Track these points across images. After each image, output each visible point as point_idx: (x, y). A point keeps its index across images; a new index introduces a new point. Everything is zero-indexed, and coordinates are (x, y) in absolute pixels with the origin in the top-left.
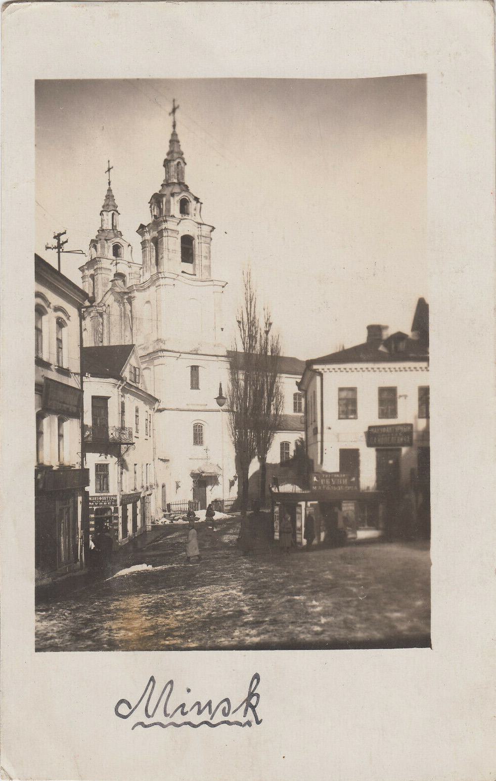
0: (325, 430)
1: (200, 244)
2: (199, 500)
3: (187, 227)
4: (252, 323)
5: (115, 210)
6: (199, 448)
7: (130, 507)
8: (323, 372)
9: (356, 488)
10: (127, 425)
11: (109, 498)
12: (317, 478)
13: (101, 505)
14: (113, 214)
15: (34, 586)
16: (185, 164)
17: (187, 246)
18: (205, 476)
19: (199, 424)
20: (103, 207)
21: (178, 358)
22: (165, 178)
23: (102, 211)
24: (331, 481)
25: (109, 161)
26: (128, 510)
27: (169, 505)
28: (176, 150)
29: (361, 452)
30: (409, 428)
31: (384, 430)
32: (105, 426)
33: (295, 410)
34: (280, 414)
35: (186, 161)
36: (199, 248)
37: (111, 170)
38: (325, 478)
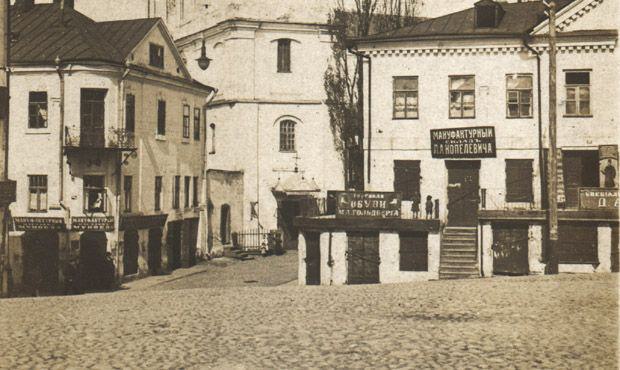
0: (374, 134)
6: (287, 156)
9: (397, 213)
12: (346, 199)
18: (290, 196)
24: (363, 203)
29: (422, 166)
30: (490, 132)
31: (453, 135)
38: (357, 200)
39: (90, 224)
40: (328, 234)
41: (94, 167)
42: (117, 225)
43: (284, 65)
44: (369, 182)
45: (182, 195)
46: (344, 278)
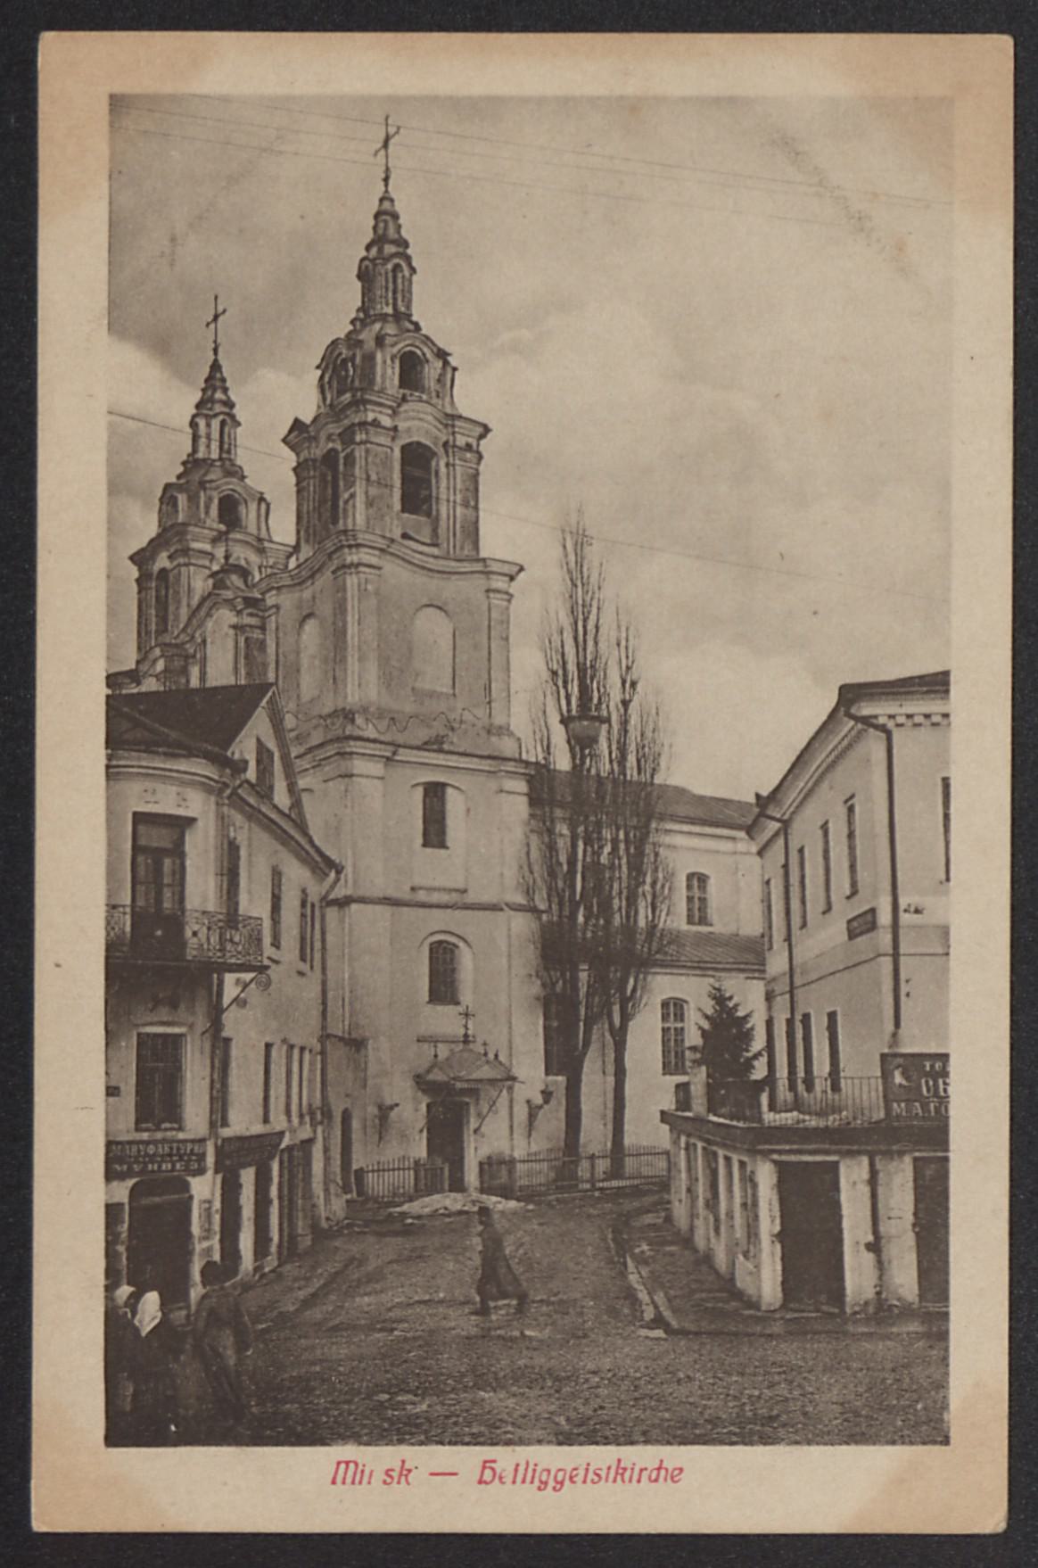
1: (451, 468)
2: (445, 1160)
3: (419, 423)
4: (586, 672)
5: (228, 414)
7: (248, 1177)
8: (891, 724)
10: (245, 905)
11: (178, 1149)
13: (153, 1171)
14: (223, 423)
15: (102, 1309)
16: (413, 270)
17: (417, 473)
19: (445, 945)
20: (198, 406)
21: (388, 759)
22: (360, 304)
23: (194, 416)
25: (216, 298)
26: (240, 1186)
27: (360, 1173)
28: (392, 233)
32: (175, 922)
33: (690, 921)
34: (661, 925)
35: (414, 264)
36: (446, 486)
37: (221, 319)
39: (152, 1158)
40: (627, 1159)
41: (164, 1013)
42: (210, 1160)
43: (434, 833)
44: (518, 1465)
45: (295, 1090)
46: (427, 999)
